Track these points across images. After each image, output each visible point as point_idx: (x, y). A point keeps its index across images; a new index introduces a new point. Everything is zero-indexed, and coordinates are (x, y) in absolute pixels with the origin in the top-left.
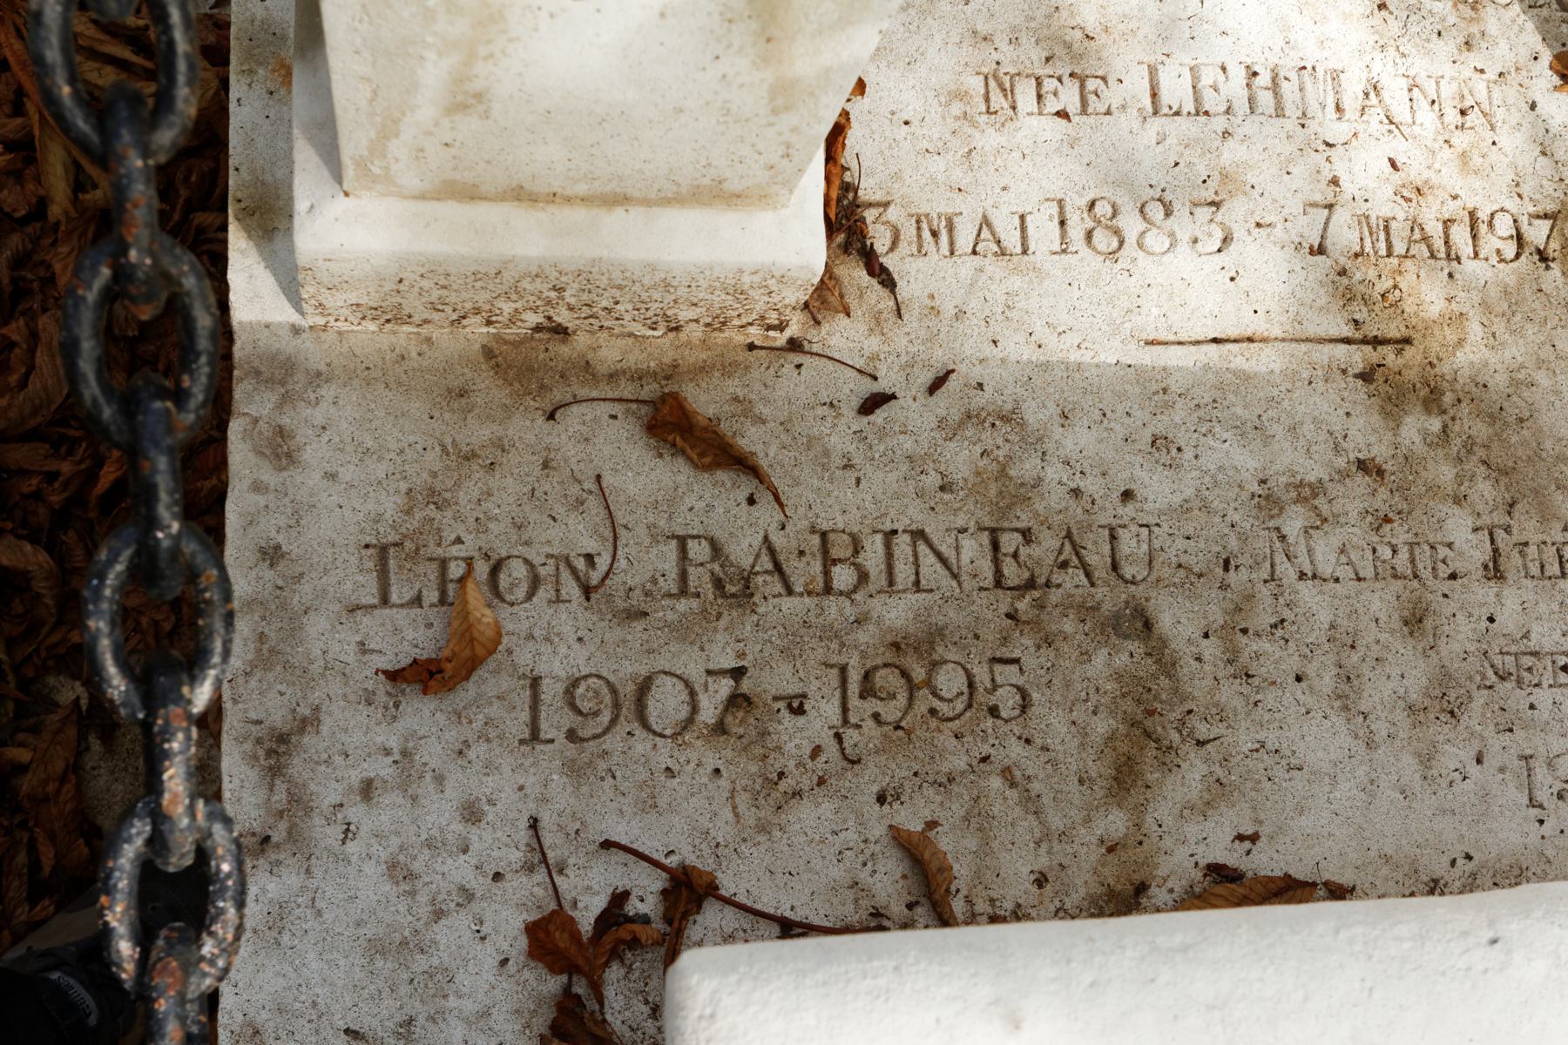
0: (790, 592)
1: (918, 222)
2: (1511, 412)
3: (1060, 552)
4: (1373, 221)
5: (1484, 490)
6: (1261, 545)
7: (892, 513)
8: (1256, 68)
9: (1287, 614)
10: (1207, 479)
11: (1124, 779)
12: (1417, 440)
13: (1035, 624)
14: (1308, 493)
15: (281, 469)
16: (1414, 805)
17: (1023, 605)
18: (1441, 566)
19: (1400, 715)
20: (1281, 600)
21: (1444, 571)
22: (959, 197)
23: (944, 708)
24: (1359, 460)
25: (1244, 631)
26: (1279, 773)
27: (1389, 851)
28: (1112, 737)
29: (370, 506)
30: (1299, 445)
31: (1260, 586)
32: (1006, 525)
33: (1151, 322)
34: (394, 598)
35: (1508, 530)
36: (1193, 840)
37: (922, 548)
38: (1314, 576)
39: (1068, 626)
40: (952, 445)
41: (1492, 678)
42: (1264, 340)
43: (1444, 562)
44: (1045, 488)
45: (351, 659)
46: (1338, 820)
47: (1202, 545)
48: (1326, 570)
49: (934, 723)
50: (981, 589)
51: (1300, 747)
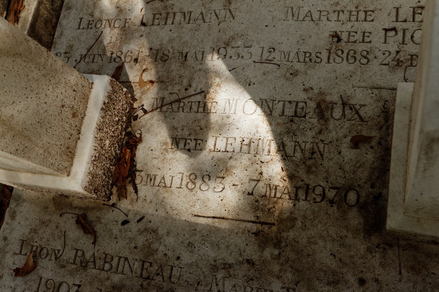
0: (95, 268)
3: (157, 270)
4: (272, 185)
5: (289, 276)
7: (122, 252)
8: (244, 139)
12: (269, 256)
14: (227, 266)
15: (12, 220)
17: (145, 283)
22: (158, 170)
29: (24, 231)
30: (229, 252)
32: (146, 260)
33: (197, 210)
34: (22, 253)
37: (126, 263)
40: (140, 236)
44: (158, 252)
45: (11, 265)
50: (136, 277)
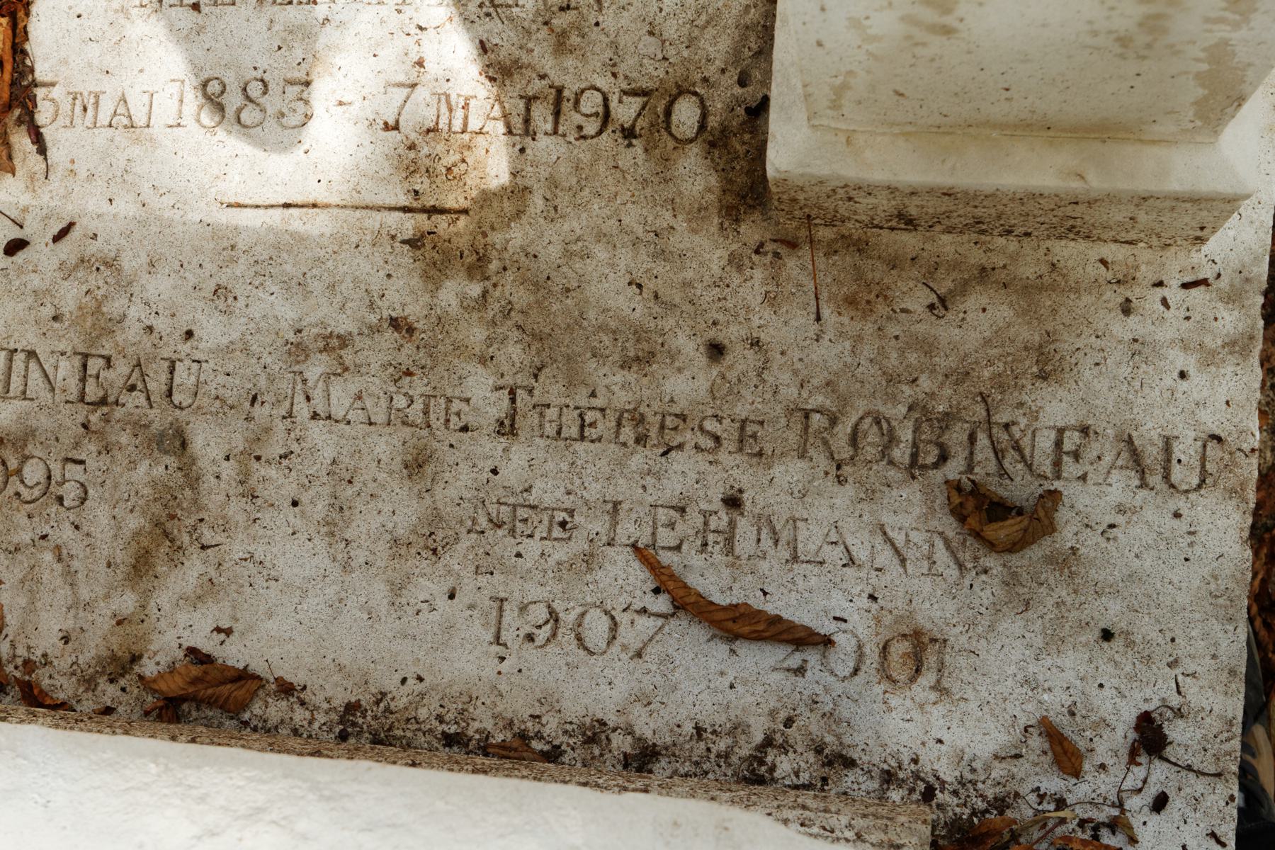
1: (74, 99)
2: (558, 281)
5: (514, 353)
6: (284, 386)
7: (16, 334)
9: (295, 447)
10: (252, 325)
11: (141, 567)
12: (454, 303)
13: (100, 434)
14: (335, 343)
16: (376, 626)
17: (94, 418)
18: (454, 419)
19: (382, 547)
20: (293, 435)
21: (455, 423)
22: (105, 78)
23: (26, 494)
24: (391, 318)
25: (258, 458)
26: (260, 581)
27: (344, 660)
28: (138, 533)
31: (278, 421)
32: (93, 352)
35: (530, 391)
36: (181, 626)
37: (33, 365)
38: (329, 417)
39: (124, 439)
40: (66, 283)
41: (483, 522)
42: (327, 206)
43: (458, 414)
44: (127, 323)
46: (300, 628)
47: (237, 382)
48: (338, 412)
49: (16, 503)
50: (67, 402)
51: (280, 562)
